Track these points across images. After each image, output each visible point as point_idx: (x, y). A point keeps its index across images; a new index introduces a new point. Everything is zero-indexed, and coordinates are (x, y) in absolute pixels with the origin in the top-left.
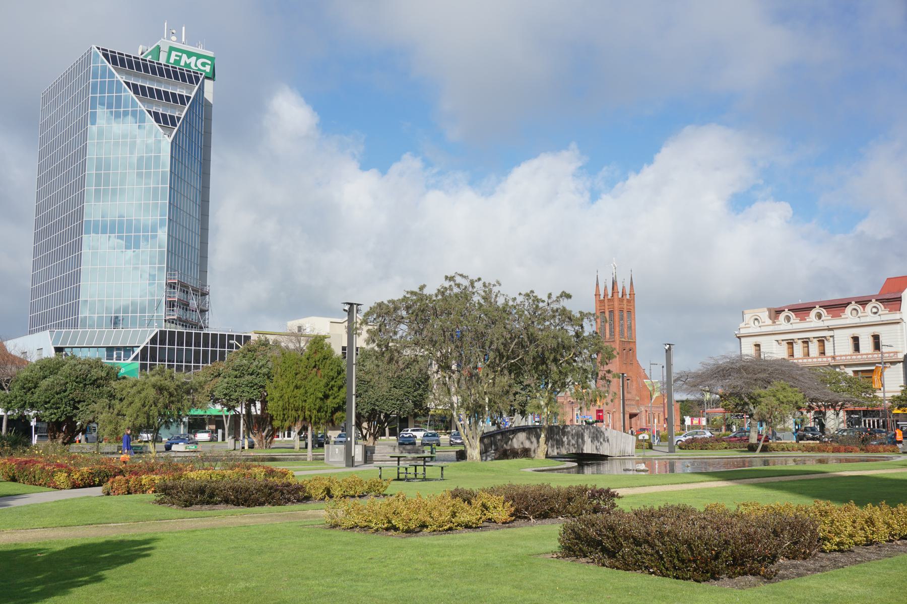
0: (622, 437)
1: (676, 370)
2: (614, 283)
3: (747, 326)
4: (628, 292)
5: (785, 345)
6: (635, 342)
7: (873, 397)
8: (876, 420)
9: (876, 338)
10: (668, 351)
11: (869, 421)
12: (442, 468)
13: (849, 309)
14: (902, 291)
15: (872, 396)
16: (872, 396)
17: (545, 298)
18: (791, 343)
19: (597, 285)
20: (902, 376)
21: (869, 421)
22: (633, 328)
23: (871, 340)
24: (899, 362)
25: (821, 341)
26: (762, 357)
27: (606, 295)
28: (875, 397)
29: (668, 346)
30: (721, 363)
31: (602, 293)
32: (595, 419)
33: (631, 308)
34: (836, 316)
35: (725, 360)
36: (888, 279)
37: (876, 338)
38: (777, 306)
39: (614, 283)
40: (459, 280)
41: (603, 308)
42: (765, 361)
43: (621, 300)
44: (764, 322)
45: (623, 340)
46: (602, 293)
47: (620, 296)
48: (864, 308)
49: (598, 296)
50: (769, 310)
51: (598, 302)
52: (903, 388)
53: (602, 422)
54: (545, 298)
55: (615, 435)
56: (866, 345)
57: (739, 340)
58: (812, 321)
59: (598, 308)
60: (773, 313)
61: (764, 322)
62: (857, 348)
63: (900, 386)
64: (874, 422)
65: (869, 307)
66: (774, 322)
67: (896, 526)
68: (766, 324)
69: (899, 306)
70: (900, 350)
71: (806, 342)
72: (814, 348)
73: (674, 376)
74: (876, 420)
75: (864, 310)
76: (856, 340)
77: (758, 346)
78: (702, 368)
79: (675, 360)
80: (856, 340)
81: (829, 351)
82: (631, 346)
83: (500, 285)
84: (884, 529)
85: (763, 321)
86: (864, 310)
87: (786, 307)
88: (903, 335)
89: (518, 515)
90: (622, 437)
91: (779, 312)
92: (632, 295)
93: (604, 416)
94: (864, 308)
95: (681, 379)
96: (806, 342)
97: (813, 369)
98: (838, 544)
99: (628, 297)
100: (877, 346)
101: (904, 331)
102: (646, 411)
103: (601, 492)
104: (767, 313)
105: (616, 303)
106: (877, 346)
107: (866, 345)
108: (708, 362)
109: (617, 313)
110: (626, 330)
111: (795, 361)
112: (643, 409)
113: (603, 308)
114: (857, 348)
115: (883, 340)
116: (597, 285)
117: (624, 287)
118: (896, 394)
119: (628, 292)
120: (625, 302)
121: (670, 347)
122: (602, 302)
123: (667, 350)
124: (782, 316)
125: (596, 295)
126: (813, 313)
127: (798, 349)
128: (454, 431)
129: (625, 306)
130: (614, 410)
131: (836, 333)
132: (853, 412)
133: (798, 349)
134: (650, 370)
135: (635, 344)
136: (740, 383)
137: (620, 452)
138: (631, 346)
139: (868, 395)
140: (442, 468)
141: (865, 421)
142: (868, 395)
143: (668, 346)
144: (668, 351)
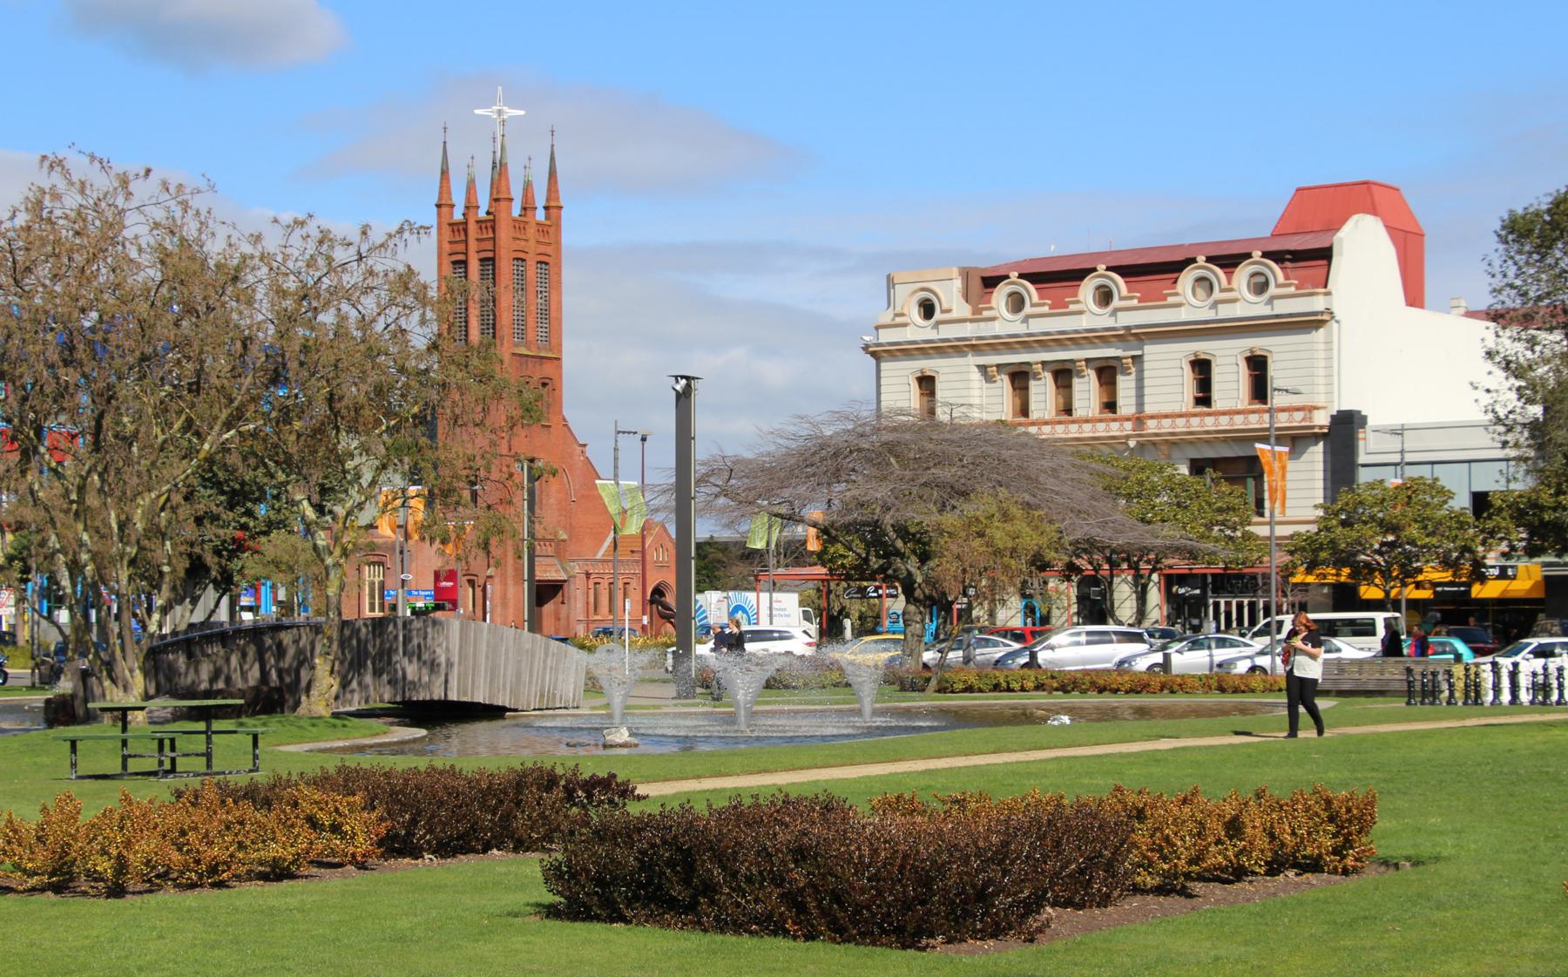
0: (546, 655)
1: (702, 451)
2: (499, 169)
3: (899, 320)
4: (540, 201)
5: (1004, 382)
6: (559, 359)
7: (1243, 537)
8: (1505, 663)
9: (1258, 365)
10: (684, 398)
11: (1228, 604)
12: (73, 743)
13: (1187, 278)
14: (1334, 226)
15: (1239, 534)
16: (1239, 534)
17: (355, 237)
18: (1020, 378)
19: (445, 173)
20: (1320, 475)
21: (1228, 604)
22: (553, 314)
23: (1244, 374)
24: (1316, 438)
25: (1107, 373)
26: (942, 415)
27: (470, 207)
28: (1248, 536)
29: (684, 382)
30: (828, 432)
31: (459, 199)
32: (431, 603)
33: (549, 250)
34: (1151, 300)
35: (840, 427)
36: (1298, 190)
37: (1258, 365)
38: (988, 262)
39: (499, 169)
40: (79, 167)
41: (461, 247)
42: (954, 427)
43: (520, 225)
44: (949, 311)
45: (523, 351)
46: (459, 199)
47: (516, 211)
48: (1229, 275)
49: (445, 210)
50: (966, 274)
51: (447, 231)
52: (1321, 513)
53: (455, 607)
54: (355, 237)
55: (528, 646)
56: (1231, 385)
57: (873, 361)
58: (1085, 311)
59: (447, 248)
60: (976, 284)
61: (949, 311)
62: (1204, 398)
63: (1316, 507)
64: (1240, 606)
65: (1243, 273)
66: (977, 311)
67: (1287, 838)
68: (954, 315)
69: (1322, 271)
70: (1320, 400)
71: (1063, 375)
72: (1086, 391)
73: (697, 470)
74: (1246, 601)
75: (1229, 282)
76: (1202, 368)
77: (927, 383)
78: (772, 448)
79: (702, 423)
80: (1202, 368)
81: (1126, 404)
82: (548, 370)
83: (212, 188)
84: (1262, 842)
85: (945, 306)
86: (1229, 282)
87: (1015, 266)
88: (1332, 393)
89: (397, 846)
90: (546, 655)
91: (991, 282)
92: (553, 211)
93: (461, 592)
94: (1229, 275)
95: (712, 480)
96: (1063, 375)
97: (1085, 450)
98: (1165, 875)
99: (540, 215)
100: (1260, 389)
101: (1335, 345)
102: (588, 575)
103: (591, 785)
104: (958, 284)
105: (505, 234)
106: (1260, 389)
107: (1231, 385)
108: (792, 429)
109: (505, 266)
110: (531, 321)
111: (1033, 430)
112: (577, 569)
113: (461, 247)
114: (1204, 398)
115: (1277, 374)
116: (445, 173)
117: (528, 188)
118: (1302, 529)
119: (540, 201)
120: (531, 231)
121: (688, 386)
122: (460, 228)
123: (678, 395)
124: (1000, 295)
125: (439, 206)
126: (1087, 289)
127: (1043, 393)
128: (1075, 619)
129: (532, 243)
130: (489, 572)
131: (1151, 351)
132: (1182, 579)
133: (1043, 393)
134: (616, 449)
135: (560, 367)
136: (881, 492)
137: (542, 696)
138: (548, 370)
139: (1228, 532)
140: (73, 743)
141: (1217, 605)
142: (1228, 532)
143: (684, 382)
144: (684, 398)
